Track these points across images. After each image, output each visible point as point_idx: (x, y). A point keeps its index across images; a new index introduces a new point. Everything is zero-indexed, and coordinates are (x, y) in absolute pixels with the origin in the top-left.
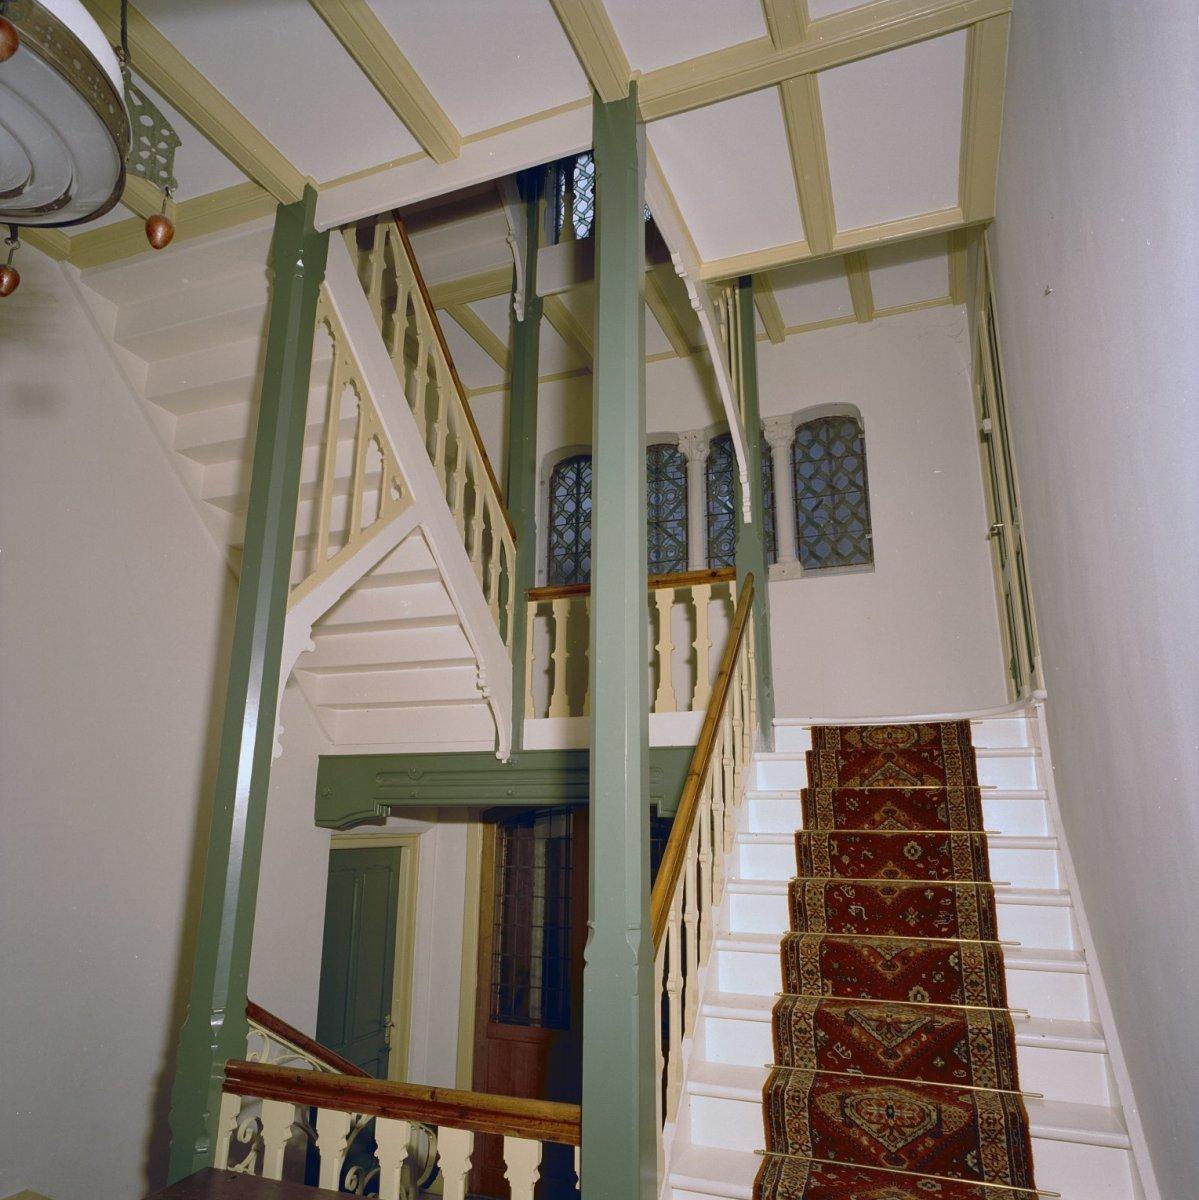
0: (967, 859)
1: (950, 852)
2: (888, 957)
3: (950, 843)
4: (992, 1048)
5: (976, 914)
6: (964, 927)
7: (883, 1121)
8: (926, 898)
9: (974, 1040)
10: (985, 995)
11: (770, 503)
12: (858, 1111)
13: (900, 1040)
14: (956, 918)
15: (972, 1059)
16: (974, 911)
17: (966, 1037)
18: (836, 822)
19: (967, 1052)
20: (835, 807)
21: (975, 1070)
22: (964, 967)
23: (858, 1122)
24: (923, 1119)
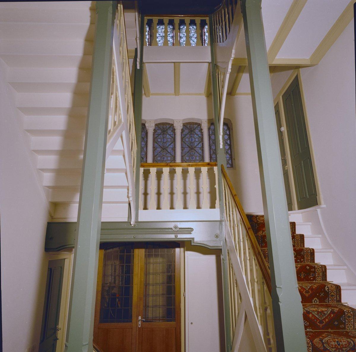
0: (309, 256)
1: (304, 254)
2: (307, 289)
3: (304, 252)
4: (352, 317)
5: (321, 273)
6: (317, 278)
7: (337, 347)
8: (307, 269)
9: (347, 315)
10: (335, 299)
11: (202, 146)
12: (328, 345)
13: (325, 317)
14: (315, 275)
15: (346, 321)
16: (321, 272)
17: (345, 314)
18: (261, 245)
19: (345, 319)
20: (261, 241)
21: (347, 324)
22: (330, 290)
23: (328, 348)
24: (349, 344)
